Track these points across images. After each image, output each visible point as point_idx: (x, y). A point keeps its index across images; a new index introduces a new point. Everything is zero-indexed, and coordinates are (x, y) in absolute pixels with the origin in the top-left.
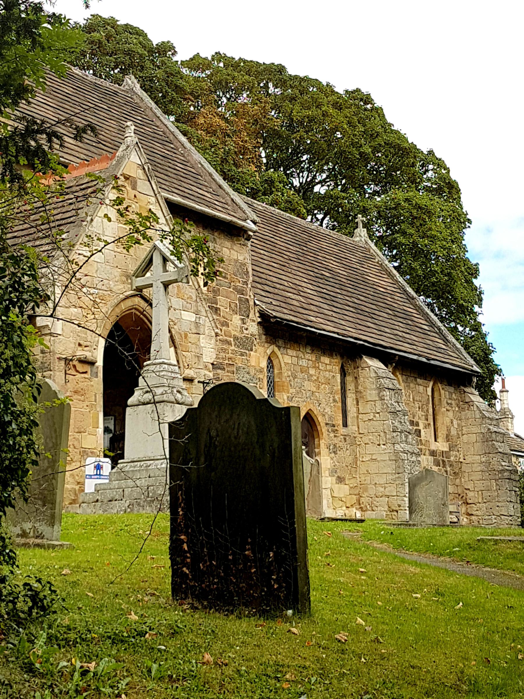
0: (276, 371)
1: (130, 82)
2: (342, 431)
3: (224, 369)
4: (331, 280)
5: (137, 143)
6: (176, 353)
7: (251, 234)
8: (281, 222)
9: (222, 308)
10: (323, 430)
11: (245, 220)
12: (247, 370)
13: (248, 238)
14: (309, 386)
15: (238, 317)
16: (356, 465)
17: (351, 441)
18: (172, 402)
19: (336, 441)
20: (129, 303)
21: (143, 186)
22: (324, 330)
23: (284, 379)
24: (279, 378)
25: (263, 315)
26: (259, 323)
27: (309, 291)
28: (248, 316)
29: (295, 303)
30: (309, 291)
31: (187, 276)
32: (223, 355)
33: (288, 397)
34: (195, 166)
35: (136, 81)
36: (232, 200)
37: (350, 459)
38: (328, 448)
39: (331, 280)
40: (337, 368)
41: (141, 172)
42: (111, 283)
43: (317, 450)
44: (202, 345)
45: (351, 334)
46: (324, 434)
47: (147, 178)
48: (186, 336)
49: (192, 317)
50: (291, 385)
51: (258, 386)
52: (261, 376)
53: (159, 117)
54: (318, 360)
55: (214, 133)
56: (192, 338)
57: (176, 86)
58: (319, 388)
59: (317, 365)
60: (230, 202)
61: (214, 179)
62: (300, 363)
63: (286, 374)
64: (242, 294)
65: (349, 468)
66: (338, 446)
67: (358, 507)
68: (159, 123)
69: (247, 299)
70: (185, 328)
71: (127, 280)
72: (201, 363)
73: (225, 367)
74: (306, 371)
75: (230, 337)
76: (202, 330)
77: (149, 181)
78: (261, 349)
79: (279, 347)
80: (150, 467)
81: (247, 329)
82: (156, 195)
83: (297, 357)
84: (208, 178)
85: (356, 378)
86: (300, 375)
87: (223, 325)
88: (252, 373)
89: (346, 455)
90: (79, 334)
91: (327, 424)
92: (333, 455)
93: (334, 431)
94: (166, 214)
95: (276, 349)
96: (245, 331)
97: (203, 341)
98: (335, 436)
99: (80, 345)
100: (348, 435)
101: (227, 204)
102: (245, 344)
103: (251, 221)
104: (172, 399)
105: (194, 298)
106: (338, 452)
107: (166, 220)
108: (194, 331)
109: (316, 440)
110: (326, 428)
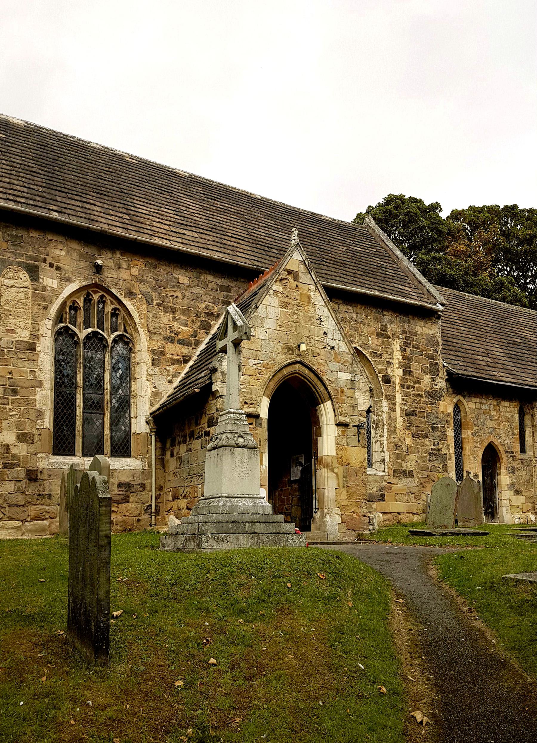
0: (462, 415)
1: (368, 220)
2: (520, 456)
3: (416, 415)
4: (522, 344)
5: (298, 244)
6: (333, 405)
7: (441, 314)
8: (486, 306)
9: (415, 371)
10: (503, 456)
11: (435, 304)
12: (437, 415)
13: (439, 317)
14: (491, 424)
15: (429, 376)
16: (532, 481)
17: (528, 464)
18: (234, 447)
19: (514, 464)
20: (291, 369)
21: (304, 277)
22: (502, 381)
23: (468, 420)
24: (465, 419)
25: (449, 373)
26: (446, 380)
27: (498, 354)
28: (437, 375)
29: (482, 363)
30: (498, 354)
31: (246, 333)
32: (415, 405)
33: (472, 433)
34: (404, 271)
35: (372, 219)
36: (428, 290)
37: (526, 477)
38: (508, 469)
39: (522, 344)
40: (516, 410)
41: (302, 267)
42: (274, 354)
43: (498, 471)
44: (357, 397)
45: (527, 383)
46: (504, 460)
47: (308, 271)
48: (342, 391)
49: (348, 376)
50: (475, 424)
51: (446, 426)
52: (449, 419)
53: (383, 241)
54: (499, 404)
55: (459, 256)
56: (348, 392)
57: (438, 230)
58: (499, 425)
59: (498, 408)
60: (426, 293)
61: (416, 278)
62: (483, 407)
63: (470, 416)
64: (433, 359)
65: (526, 483)
66: (516, 467)
67: (533, 512)
68: (383, 245)
69: (437, 363)
70: (341, 385)
71: (288, 351)
72: (356, 412)
73: (417, 413)
74: (488, 413)
75: (422, 391)
76: (357, 386)
77: (310, 273)
78: (448, 399)
79: (464, 397)
80: (211, 505)
81: (436, 385)
82: (315, 283)
83: (480, 403)
84: (412, 278)
85: (532, 416)
86: (483, 416)
87: (415, 383)
88: (441, 416)
89: (523, 474)
90: (246, 395)
91: (506, 452)
92: (511, 474)
93: (512, 457)
94: (324, 298)
95: (462, 398)
96: (435, 387)
97: (358, 394)
98: (513, 461)
99: (246, 403)
100: (525, 459)
101: (423, 294)
102: (435, 396)
103: (440, 304)
104: (232, 443)
105: (350, 361)
106: (516, 472)
107: (325, 302)
108: (350, 387)
109: (498, 464)
110: (506, 455)
